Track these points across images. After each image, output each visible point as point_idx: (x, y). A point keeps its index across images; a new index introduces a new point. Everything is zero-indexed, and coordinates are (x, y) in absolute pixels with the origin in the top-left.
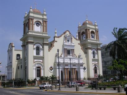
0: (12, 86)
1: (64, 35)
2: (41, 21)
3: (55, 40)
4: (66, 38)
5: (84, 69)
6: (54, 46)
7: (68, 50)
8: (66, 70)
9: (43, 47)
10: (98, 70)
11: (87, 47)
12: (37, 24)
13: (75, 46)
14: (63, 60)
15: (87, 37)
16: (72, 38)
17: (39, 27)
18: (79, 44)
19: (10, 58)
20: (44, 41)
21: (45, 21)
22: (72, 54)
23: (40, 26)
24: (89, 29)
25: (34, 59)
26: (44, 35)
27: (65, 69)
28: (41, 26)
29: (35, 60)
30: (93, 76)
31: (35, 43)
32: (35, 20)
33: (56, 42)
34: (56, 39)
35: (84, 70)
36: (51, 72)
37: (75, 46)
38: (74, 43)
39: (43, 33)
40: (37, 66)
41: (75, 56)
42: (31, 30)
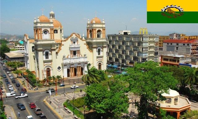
13: (80, 47)
29: (45, 64)
37: (80, 47)
39: (50, 41)
41: (80, 55)
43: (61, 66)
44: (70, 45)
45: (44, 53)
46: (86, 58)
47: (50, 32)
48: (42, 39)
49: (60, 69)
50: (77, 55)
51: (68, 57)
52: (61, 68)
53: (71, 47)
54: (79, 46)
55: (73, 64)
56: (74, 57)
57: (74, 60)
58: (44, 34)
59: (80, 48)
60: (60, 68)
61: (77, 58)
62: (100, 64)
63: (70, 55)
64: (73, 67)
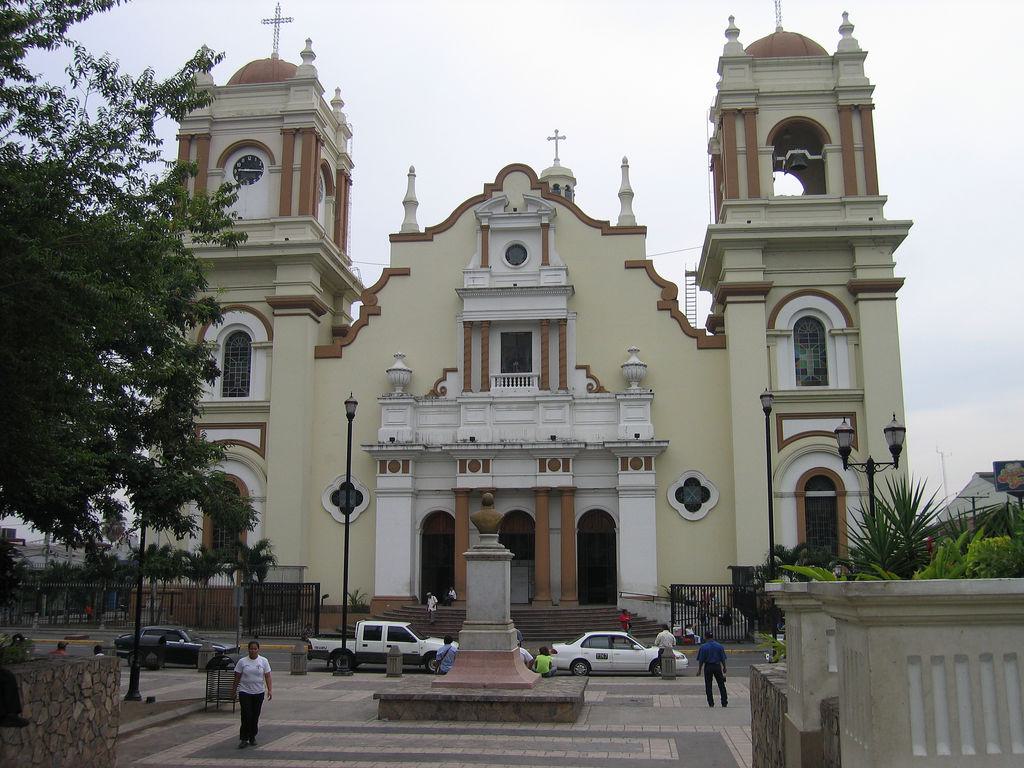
2: (272, 140)
51: (437, 393)
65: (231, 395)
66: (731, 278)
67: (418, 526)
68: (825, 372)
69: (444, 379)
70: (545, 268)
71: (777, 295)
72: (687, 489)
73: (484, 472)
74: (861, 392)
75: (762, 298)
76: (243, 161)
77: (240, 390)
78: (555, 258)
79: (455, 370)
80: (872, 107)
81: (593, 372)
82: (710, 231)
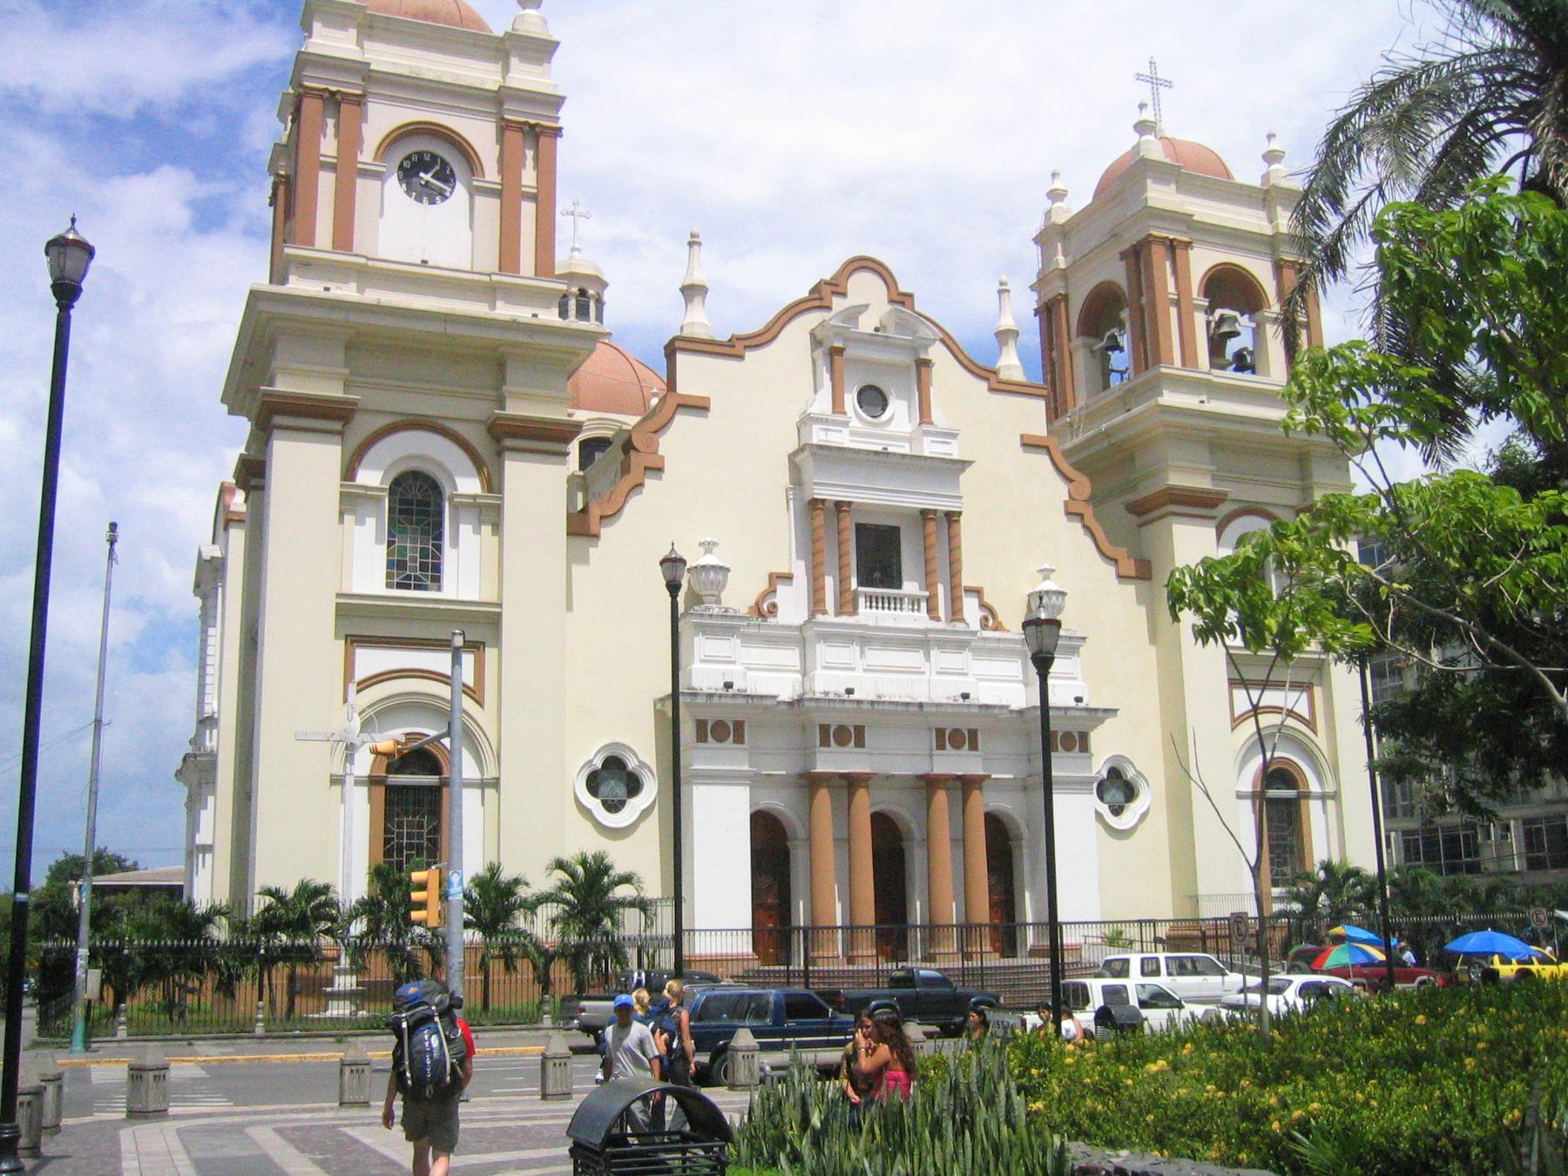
0: (1410, 860)
1: (812, 320)
2: (480, 133)
3: (684, 387)
4: (835, 353)
5: (1116, 795)
6: (657, 470)
7: (860, 528)
8: (941, 797)
9: (493, 484)
10: (1314, 807)
11: (1146, 490)
12: (409, 172)
13: (964, 464)
14: (791, 656)
15: (1148, 353)
16: (923, 364)
17: (441, 207)
18: (1029, 444)
19: (223, 627)
20: (501, 402)
21: (524, 128)
22: (929, 585)
23: (460, 192)
24: (1172, 246)
25: (355, 641)
26: (505, 311)
27: (811, 782)
28: (474, 192)
29: (371, 661)
30: (1240, 896)
31: (381, 422)
32: (382, 118)
33: (700, 407)
34: (694, 374)
35: (1117, 811)
36: (602, 828)
37: (964, 464)
38: (951, 435)
39: (491, 291)
40: (389, 738)
41: (970, 607)
42: (1178, 362)
43: (644, 753)
44: (806, 420)
45: (371, 477)
46: (1041, 571)
47: (492, 174)
48: (360, 243)
49: (635, 806)
50: (910, 587)
51: (763, 610)
52: (650, 791)
53: (818, 436)
54: (953, 451)
55: (849, 734)
56: (866, 615)
57: (878, 656)
58: (394, 186)
59: (965, 478)
60: (1130, 792)
61: (921, 642)
62: (419, 757)
63: (799, 569)
64: (851, 783)
65: (400, 586)
66: (284, 385)
67: (1522, 838)
68: (437, 568)
69: (772, 591)
70: (925, 427)
71: (363, 426)
72: (605, 774)
73: (1081, 751)
74: (498, 610)
75: (338, 426)
76: (415, 158)
77: (416, 578)
78: (936, 414)
79: (787, 578)
80: (557, 132)
81: (987, 599)
82: (255, 296)
